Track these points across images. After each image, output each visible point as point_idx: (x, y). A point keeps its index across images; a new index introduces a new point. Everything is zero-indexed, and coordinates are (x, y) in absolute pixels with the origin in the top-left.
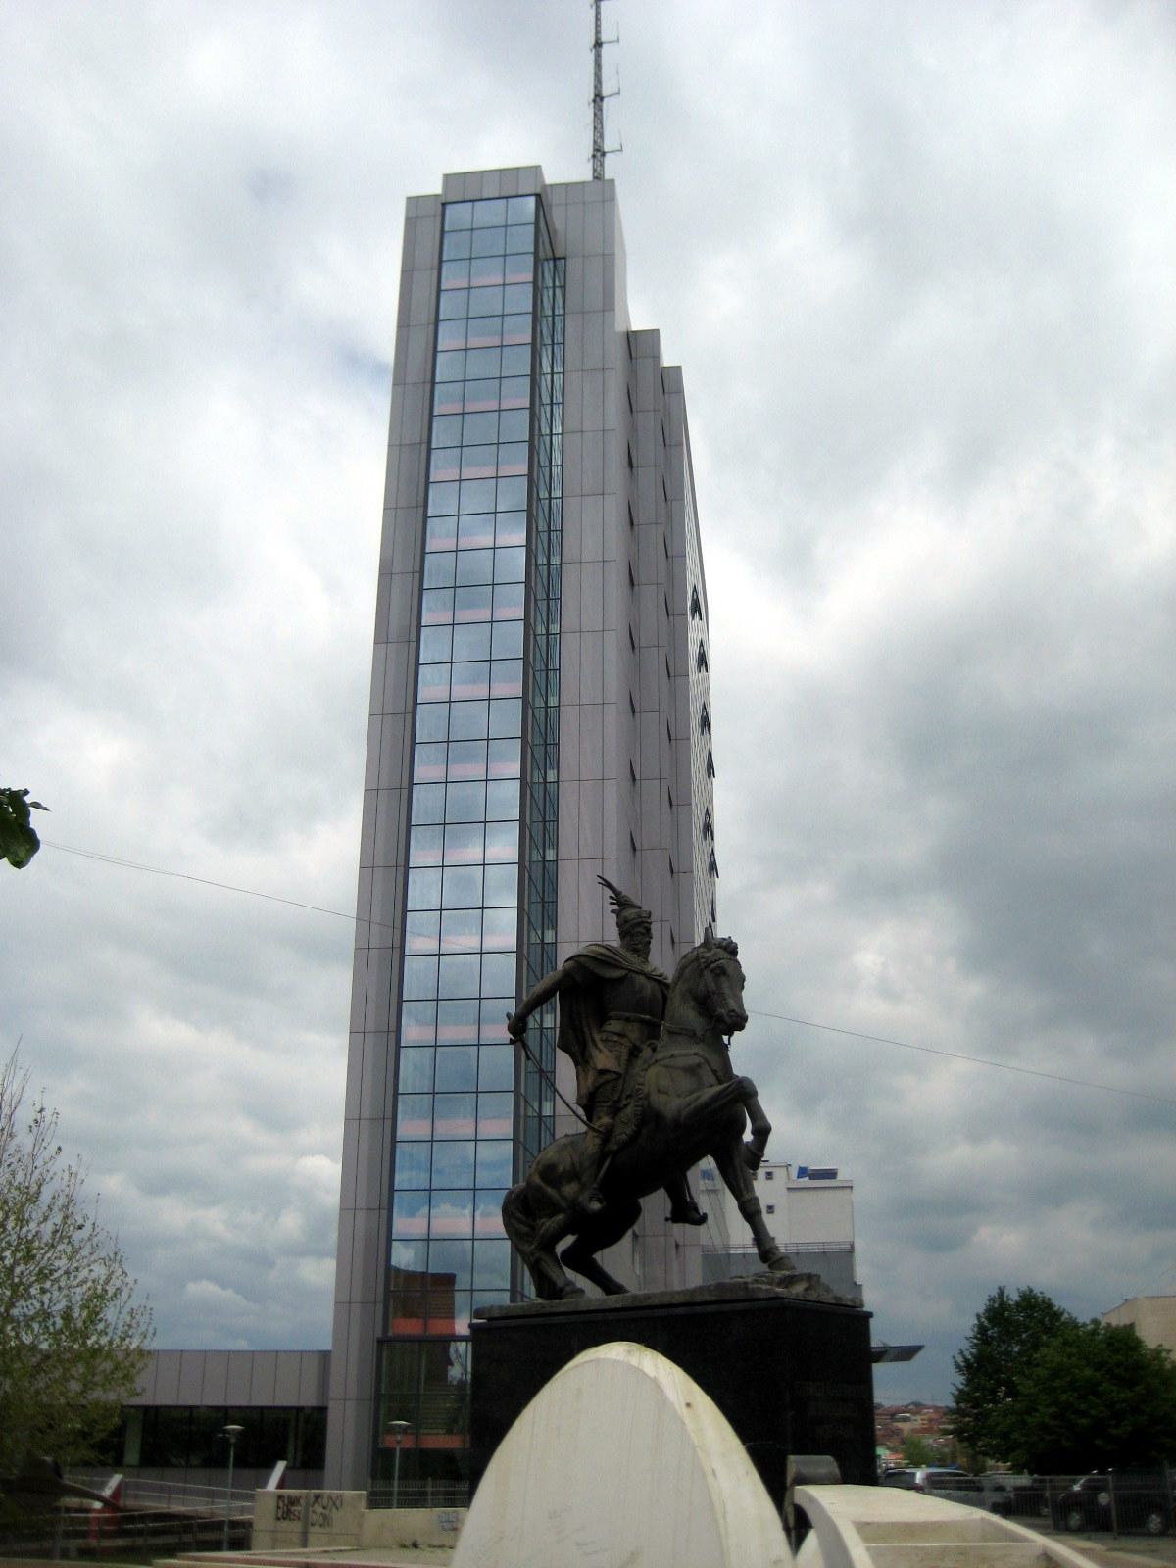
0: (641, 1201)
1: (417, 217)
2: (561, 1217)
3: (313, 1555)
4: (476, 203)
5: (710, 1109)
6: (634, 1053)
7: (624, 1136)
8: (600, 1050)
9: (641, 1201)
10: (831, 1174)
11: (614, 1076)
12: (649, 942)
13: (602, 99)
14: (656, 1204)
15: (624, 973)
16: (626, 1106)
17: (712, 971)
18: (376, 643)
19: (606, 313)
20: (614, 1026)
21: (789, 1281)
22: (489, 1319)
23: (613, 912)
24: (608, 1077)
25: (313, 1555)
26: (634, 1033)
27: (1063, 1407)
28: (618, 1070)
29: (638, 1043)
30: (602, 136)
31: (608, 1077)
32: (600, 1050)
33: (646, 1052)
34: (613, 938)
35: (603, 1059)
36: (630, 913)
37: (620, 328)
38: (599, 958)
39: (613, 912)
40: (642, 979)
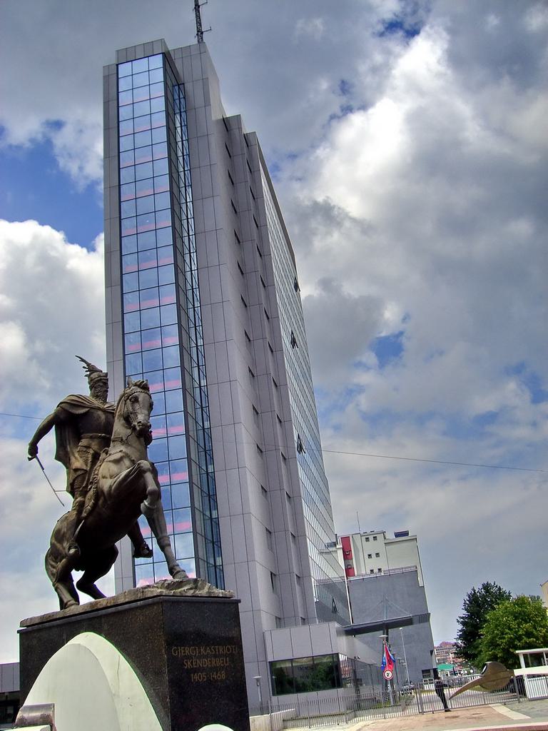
0: (117, 544)
1: (109, 76)
2: (64, 560)
3: (320, 730)
4: (134, 62)
5: (125, 483)
6: (96, 457)
7: (89, 507)
8: (76, 458)
9: (117, 544)
10: (406, 534)
11: (82, 472)
12: (107, 391)
13: (199, 7)
14: (124, 545)
15: (87, 409)
16: (90, 489)
17: (130, 400)
18: (106, 287)
19: (207, 107)
20: (84, 442)
21: (180, 584)
22: (27, 626)
23: (86, 376)
24: (79, 473)
25: (320, 730)
26: (95, 446)
27: (498, 639)
28: (85, 468)
29: (99, 451)
30: (201, 25)
31: (79, 473)
32: (76, 458)
33: (103, 455)
34: (86, 391)
35: (78, 463)
36: (95, 375)
37: (216, 116)
38: (72, 402)
39: (86, 376)
40: (100, 413)
